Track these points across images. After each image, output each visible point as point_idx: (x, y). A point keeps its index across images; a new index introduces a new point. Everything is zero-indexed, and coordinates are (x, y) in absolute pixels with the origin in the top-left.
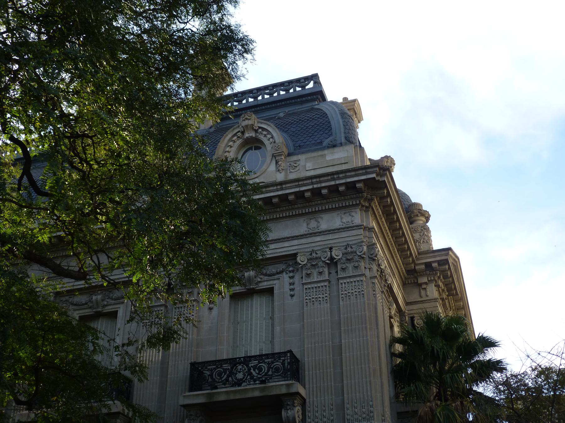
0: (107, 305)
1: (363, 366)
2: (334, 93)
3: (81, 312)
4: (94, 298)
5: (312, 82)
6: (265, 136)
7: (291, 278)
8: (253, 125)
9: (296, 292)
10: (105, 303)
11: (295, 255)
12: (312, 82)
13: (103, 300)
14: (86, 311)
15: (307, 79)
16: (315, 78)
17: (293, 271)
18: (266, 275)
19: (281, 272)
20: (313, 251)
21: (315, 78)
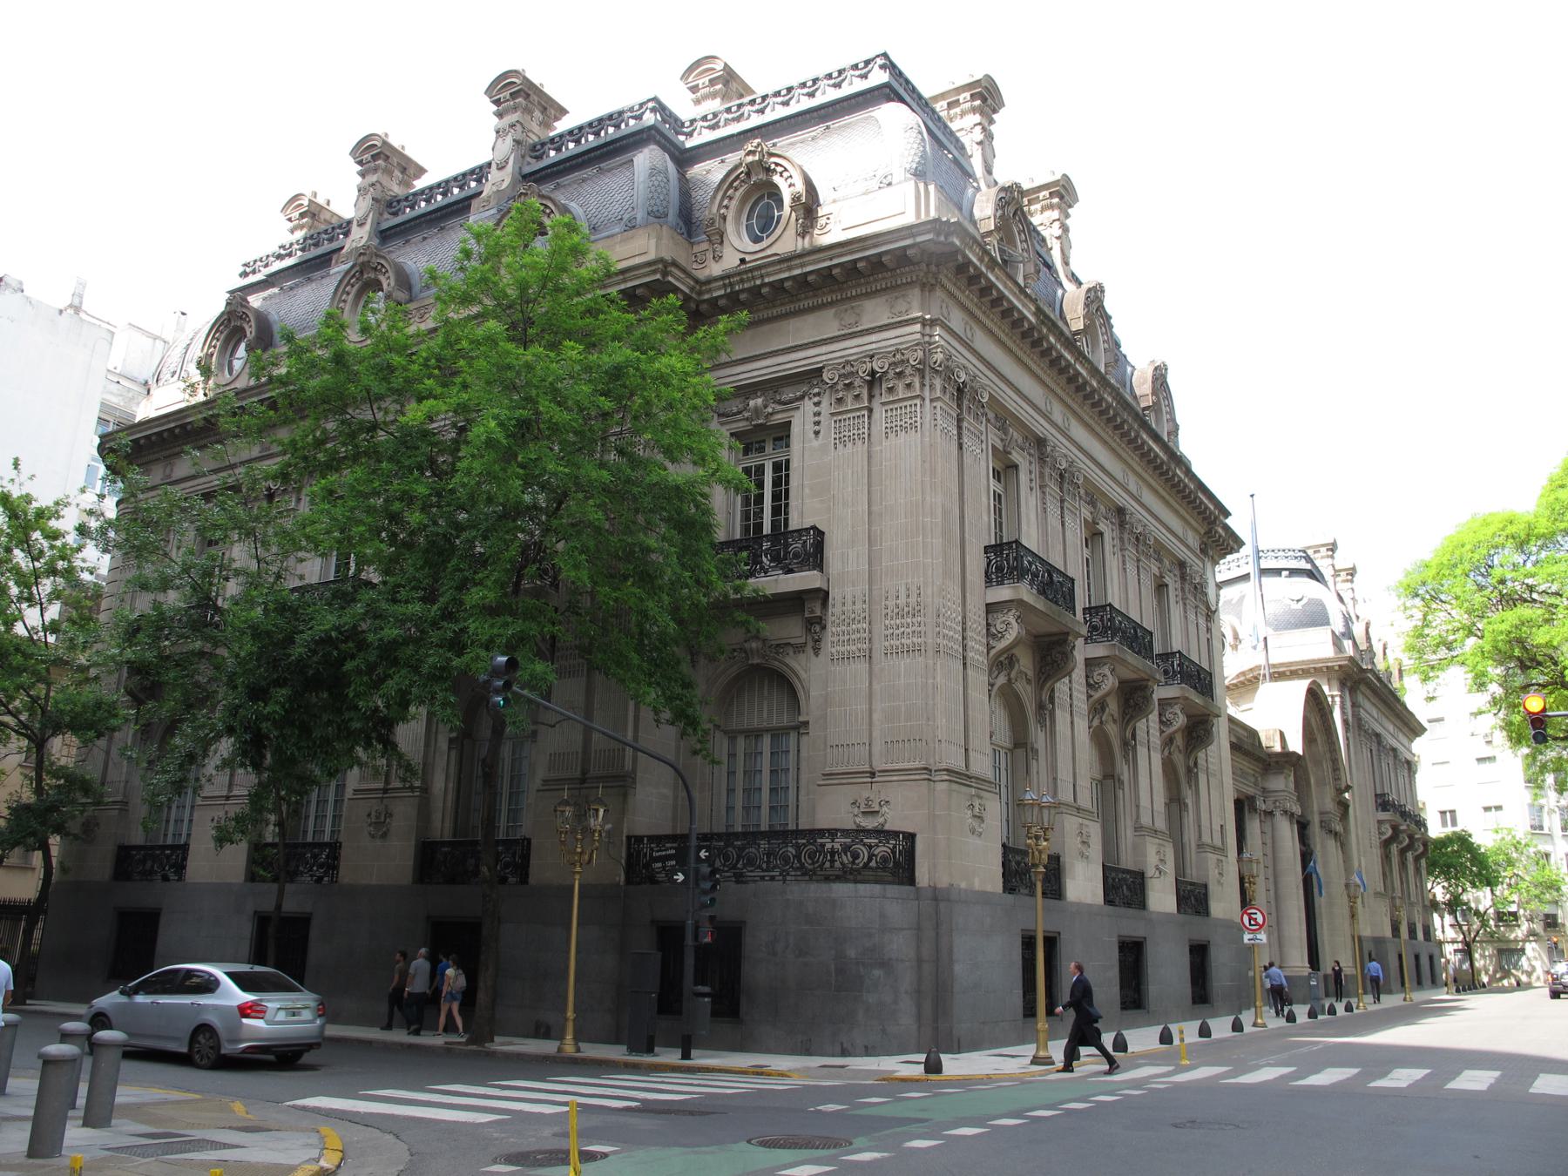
4: (752, 403)
9: (822, 428)
10: (770, 410)
11: (820, 370)
17: (818, 394)
19: (802, 398)
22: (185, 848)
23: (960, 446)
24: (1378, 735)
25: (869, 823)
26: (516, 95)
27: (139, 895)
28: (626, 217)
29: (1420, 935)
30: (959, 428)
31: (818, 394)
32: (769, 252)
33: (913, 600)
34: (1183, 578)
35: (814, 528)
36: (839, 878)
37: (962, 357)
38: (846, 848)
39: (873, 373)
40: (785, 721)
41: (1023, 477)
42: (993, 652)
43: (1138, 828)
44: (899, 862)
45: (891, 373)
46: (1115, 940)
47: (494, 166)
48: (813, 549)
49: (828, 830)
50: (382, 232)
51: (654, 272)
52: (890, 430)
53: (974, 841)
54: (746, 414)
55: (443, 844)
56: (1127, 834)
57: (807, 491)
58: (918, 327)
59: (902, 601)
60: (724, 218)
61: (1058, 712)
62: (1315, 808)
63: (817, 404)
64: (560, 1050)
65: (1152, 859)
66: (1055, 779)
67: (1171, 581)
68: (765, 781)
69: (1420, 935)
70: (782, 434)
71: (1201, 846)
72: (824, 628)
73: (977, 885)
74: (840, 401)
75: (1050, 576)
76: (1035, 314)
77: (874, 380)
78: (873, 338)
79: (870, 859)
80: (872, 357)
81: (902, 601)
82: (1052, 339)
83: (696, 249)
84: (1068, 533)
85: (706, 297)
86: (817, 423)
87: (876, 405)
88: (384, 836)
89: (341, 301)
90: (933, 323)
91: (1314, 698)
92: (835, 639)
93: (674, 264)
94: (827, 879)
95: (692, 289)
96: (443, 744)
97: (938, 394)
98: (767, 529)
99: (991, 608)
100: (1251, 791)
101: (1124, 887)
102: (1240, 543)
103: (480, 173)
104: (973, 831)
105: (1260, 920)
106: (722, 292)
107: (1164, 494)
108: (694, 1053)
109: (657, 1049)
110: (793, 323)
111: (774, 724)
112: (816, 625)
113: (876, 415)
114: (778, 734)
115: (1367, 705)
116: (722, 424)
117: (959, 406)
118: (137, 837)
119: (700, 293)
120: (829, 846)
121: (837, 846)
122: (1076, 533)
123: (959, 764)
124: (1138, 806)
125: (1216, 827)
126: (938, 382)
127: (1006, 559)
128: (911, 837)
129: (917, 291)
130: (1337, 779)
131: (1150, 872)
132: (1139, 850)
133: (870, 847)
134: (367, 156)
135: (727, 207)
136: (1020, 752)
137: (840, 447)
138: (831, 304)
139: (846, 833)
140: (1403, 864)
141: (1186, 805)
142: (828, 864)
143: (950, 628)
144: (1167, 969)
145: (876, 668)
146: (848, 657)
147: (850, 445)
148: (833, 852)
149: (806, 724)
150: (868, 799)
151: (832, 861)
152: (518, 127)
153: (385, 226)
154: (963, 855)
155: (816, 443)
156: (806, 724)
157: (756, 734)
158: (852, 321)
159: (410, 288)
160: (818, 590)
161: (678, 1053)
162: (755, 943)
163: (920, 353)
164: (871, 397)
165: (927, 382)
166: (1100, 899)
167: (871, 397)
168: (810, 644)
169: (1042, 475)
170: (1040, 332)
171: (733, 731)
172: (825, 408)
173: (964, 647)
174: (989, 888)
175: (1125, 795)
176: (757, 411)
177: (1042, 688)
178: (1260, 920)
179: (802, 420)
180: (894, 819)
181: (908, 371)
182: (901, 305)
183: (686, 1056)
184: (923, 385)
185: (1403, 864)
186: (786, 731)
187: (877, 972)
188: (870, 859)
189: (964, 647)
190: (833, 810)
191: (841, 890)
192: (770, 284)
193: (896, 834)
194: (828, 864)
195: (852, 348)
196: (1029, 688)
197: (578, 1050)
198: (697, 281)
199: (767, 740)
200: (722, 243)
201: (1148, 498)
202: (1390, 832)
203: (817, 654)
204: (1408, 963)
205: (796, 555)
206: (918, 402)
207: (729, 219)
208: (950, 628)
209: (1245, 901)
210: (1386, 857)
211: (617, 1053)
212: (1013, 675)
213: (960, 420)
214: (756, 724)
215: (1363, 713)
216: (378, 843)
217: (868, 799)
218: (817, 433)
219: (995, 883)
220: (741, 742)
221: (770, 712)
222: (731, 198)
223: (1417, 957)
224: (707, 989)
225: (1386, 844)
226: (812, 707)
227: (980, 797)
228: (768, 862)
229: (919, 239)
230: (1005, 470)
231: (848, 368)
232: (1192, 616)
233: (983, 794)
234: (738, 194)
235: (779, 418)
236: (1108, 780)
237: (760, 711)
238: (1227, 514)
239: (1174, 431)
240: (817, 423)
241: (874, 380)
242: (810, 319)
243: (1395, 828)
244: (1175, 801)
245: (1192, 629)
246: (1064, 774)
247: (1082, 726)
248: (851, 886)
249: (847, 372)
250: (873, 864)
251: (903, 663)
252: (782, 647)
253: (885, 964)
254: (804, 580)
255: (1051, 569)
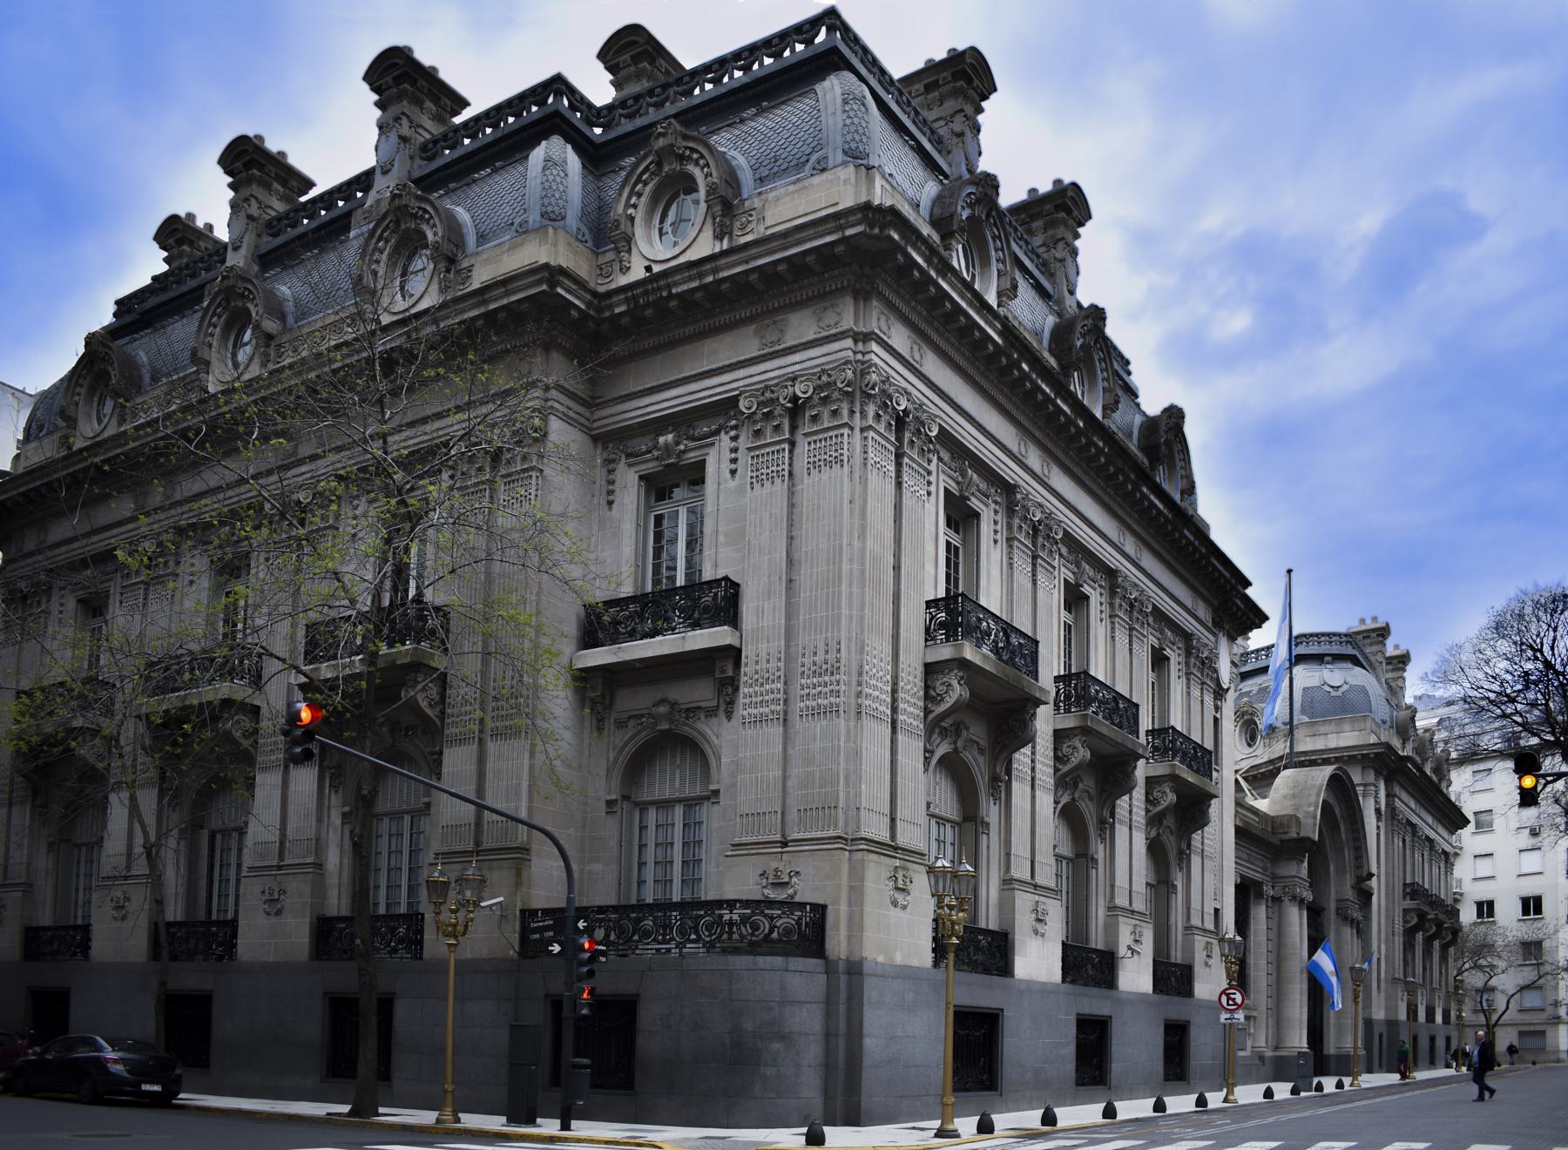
0: (684, 452)
1: (855, 590)
2: (182, 214)
3: (643, 467)
4: (662, 440)
5: (824, 29)
6: (697, 164)
7: (734, 439)
8: (672, 145)
9: (740, 466)
10: (682, 447)
11: (735, 399)
12: (824, 29)
13: (678, 444)
14: (650, 465)
15: (814, 23)
16: (831, 17)
17: (735, 427)
18: (694, 439)
19: (717, 432)
20: (767, 387)
21: (831, 17)
22: (86, 929)
23: (899, 484)
24: (1413, 826)
25: (781, 895)
26: (399, 78)
27: (190, 977)
28: (517, 221)
29: (1439, 1019)
30: (899, 465)
31: (735, 427)
32: (682, 260)
33: (831, 657)
34: (1188, 653)
35: (726, 579)
36: (736, 951)
37: (901, 377)
38: (744, 919)
39: (795, 399)
40: (698, 791)
41: (986, 527)
42: (931, 716)
43: (1112, 908)
44: (808, 933)
45: (816, 399)
46: (1072, 1019)
47: (378, 172)
48: (723, 603)
49: (727, 901)
50: (261, 257)
51: (539, 282)
52: (814, 465)
53: (895, 913)
54: (656, 453)
55: (339, 919)
56: (1099, 913)
57: (721, 538)
58: (848, 343)
59: (819, 659)
60: (632, 219)
61: (1015, 785)
62: (1333, 895)
63: (734, 439)
64: (438, 1121)
65: (1125, 939)
66: (1008, 855)
67: (1175, 657)
68: (677, 854)
69: (1439, 1019)
70: (695, 476)
71: (1189, 928)
72: (737, 689)
73: (899, 959)
74: (758, 434)
75: (1007, 636)
76: (1000, 334)
77: (796, 409)
78: (797, 357)
79: (771, 931)
80: (794, 379)
81: (819, 659)
82: (1025, 366)
83: (602, 260)
84: (1040, 594)
85: (607, 314)
86: (734, 461)
87: (799, 438)
88: (279, 913)
89: (206, 335)
90: (867, 337)
91: (1339, 785)
92: (747, 701)
93: (562, 271)
94: (724, 951)
95: (589, 304)
96: (336, 819)
97: (870, 422)
98: (680, 581)
99: (931, 670)
100: (1257, 876)
101: (1088, 964)
102: (1266, 618)
103: (363, 181)
104: (895, 903)
105: (1239, 1000)
106: (623, 308)
107: (1168, 558)
108: (574, 1124)
109: (539, 1120)
110: (710, 344)
111: (687, 793)
112: (729, 687)
113: (798, 450)
114: (691, 803)
115: (1405, 796)
116: (630, 465)
117: (899, 439)
118: (45, 918)
119: (599, 310)
120: (726, 917)
121: (735, 917)
122: (1052, 597)
123: (883, 835)
124: (1113, 886)
125: (1210, 911)
126: (871, 409)
127: (954, 613)
128: (820, 910)
129: (849, 301)
130: (1359, 867)
131: (1122, 951)
132: (1111, 930)
133: (772, 918)
134: (239, 164)
135: (635, 206)
136: (970, 826)
137: (757, 486)
138: (751, 319)
139: (746, 903)
140: (1428, 952)
141: (1175, 887)
142: (725, 936)
143: (875, 688)
144: (1136, 1044)
145: (791, 731)
146: (760, 721)
147: (768, 484)
148: (731, 923)
149: (716, 793)
150: (776, 870)
151: (730, 933)
152: (405, 121)
153: (264, 249)
154: (895, 931)
155: (732, 484)
156: (716, 793)
157: (665, 805)
158: (775, 339)
159: (283, 317)
160: (729, 647)
161: (557, 1123)
162: (649, 1015)
163: (850, 373)
164: (793, 428)
165: (857, 409)
166: (1056, 974)
167: (793, 428)
168: (723, 707)
169: (1010, 527)
170: (1009, 357)
171: (645, 803)
172: (743, 443)
173: (894, 710)
174: (914, 963)
175: (1098, 876)
176: (667, 448)
177: (996, 759)
178: (1239, 1000)
179: (716, 461)
180: (805, 891)
181: (836, 395)
182: (830, 318)
183: (565, 1126)
184: (852, 412)
185: (1428, 952)
186: (691, 803)
187: (776, 1046)
188: (771, 931)
189: (894, 710)
190: (733, 880)
191: (740, 962)
192: (678, 294)
193: (802, 905)
194: (725, 936)
195: (772, 370)
196: (981, 759)
197: (458, 1121)
198: (595, 294)
199: (679, 811)
200: (629, 251)
201: (1148, 562)
202: (1415, 920)
203: (729, 718)
204: (1424, 1043)
205: (706, 610)
206: (846, 431)
207: (638, 220)
208: (875, 688)
209: (1240, 978)
210: (1409, 946)
211: (496, 1123)
212: (960, 744)
213: (899, 456)
214: (667, 795)
215: (1398, 803)
216: (273, 920)
217: (776, 870)
218: (733, 472)
219: (927, 959)
220: (652, 814)
221: (682, 781)
222: (639, 195)
223: (1432, 1039)
224: (585, 1061)
225: (1409, 933)
226: (722, 777)
227: (904, 868)
228: (664, 935)
229: (849, 232)
230: (960, 516)
231: (768, 395)
232: (1196, 692)
233: (910, 865)
234: (648, 189)
235: (692, 456)
236: (1079, 862)
237: (672, 780)
238: (1248, 584)
239: (1190, 490)
240: (734, 461)
241: (796, 409)
242: (727, 338)
243: (1422, 916)
244: (1162, 886)
245: (1196, 706)
246: (1020, 847)
247: (1046, 802)
248: (750, 958)
249: (766, 394)
250: (775, 935)
251: (819, 726)
252: (693, 711)
253: (784, 1037)
254: (719, 636)
255: (1008, 629)
